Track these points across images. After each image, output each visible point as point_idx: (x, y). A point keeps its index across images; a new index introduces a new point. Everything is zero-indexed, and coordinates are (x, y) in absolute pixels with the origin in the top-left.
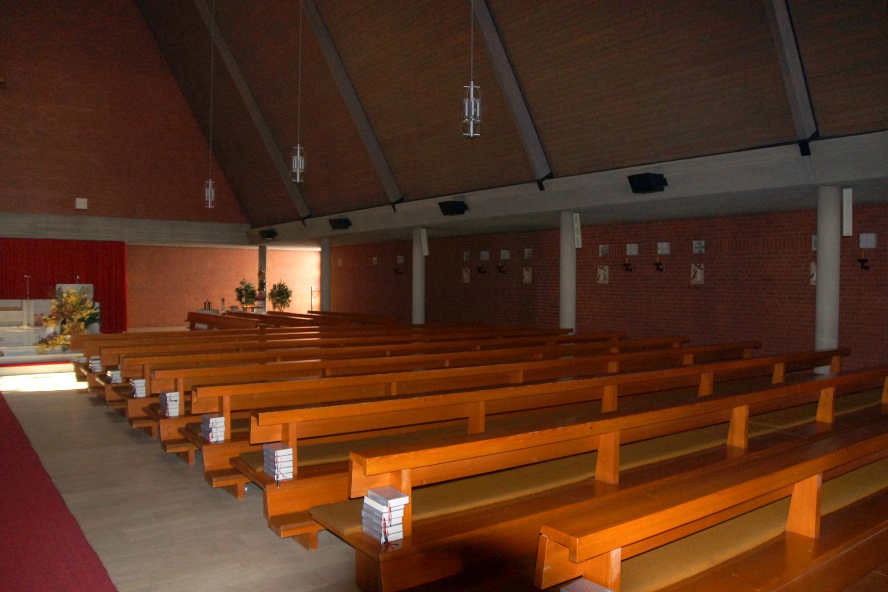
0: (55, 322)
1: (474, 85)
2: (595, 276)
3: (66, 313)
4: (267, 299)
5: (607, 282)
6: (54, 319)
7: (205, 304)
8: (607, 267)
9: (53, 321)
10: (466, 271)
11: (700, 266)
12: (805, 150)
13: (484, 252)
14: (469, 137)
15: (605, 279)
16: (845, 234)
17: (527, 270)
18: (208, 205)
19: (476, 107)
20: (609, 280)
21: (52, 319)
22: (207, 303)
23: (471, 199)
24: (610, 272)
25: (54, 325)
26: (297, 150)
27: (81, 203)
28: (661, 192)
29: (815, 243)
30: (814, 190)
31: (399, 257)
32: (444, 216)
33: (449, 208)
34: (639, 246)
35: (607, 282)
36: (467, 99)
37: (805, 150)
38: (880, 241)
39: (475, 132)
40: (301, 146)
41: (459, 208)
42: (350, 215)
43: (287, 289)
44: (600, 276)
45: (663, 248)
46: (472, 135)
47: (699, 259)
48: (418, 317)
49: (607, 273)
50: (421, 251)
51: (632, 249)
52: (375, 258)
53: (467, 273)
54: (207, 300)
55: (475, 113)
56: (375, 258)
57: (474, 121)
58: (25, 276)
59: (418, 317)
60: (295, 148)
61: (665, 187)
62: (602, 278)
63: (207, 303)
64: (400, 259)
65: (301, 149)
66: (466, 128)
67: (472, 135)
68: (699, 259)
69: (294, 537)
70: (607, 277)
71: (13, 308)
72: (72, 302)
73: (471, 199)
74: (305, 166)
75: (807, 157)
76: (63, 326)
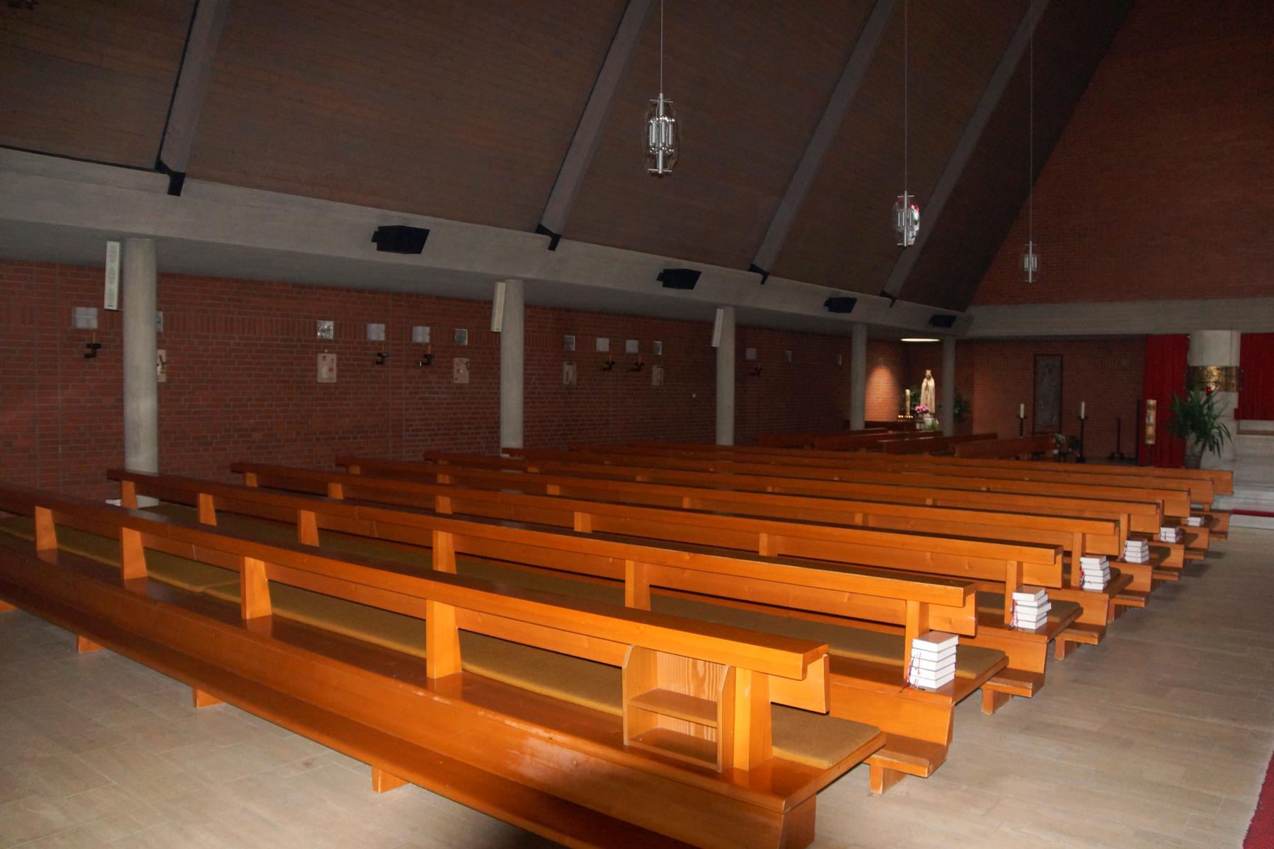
2: (313, 368)
4: (909, 397)
11: (1207, 414)
12: (175, 188)
14: (656, 174)
28: (416, 255)
29: (159, 322)
32: (694, 290)
33: (673, 278)
34: (595, 348)
39: (665, 166)
41: (685, 279)
42: (824, 313)
46: (660, 172)
48: (725, 435)
51: (377, 332)
57: (664, 152)
59: (725, 435)
60: (1026, 245)
61: (375, 245)
64: (751, 354)
67: (660, 172)
69: (1068, 627)
71: (758, 516)
75: (174, 197)
76: (632, 595)
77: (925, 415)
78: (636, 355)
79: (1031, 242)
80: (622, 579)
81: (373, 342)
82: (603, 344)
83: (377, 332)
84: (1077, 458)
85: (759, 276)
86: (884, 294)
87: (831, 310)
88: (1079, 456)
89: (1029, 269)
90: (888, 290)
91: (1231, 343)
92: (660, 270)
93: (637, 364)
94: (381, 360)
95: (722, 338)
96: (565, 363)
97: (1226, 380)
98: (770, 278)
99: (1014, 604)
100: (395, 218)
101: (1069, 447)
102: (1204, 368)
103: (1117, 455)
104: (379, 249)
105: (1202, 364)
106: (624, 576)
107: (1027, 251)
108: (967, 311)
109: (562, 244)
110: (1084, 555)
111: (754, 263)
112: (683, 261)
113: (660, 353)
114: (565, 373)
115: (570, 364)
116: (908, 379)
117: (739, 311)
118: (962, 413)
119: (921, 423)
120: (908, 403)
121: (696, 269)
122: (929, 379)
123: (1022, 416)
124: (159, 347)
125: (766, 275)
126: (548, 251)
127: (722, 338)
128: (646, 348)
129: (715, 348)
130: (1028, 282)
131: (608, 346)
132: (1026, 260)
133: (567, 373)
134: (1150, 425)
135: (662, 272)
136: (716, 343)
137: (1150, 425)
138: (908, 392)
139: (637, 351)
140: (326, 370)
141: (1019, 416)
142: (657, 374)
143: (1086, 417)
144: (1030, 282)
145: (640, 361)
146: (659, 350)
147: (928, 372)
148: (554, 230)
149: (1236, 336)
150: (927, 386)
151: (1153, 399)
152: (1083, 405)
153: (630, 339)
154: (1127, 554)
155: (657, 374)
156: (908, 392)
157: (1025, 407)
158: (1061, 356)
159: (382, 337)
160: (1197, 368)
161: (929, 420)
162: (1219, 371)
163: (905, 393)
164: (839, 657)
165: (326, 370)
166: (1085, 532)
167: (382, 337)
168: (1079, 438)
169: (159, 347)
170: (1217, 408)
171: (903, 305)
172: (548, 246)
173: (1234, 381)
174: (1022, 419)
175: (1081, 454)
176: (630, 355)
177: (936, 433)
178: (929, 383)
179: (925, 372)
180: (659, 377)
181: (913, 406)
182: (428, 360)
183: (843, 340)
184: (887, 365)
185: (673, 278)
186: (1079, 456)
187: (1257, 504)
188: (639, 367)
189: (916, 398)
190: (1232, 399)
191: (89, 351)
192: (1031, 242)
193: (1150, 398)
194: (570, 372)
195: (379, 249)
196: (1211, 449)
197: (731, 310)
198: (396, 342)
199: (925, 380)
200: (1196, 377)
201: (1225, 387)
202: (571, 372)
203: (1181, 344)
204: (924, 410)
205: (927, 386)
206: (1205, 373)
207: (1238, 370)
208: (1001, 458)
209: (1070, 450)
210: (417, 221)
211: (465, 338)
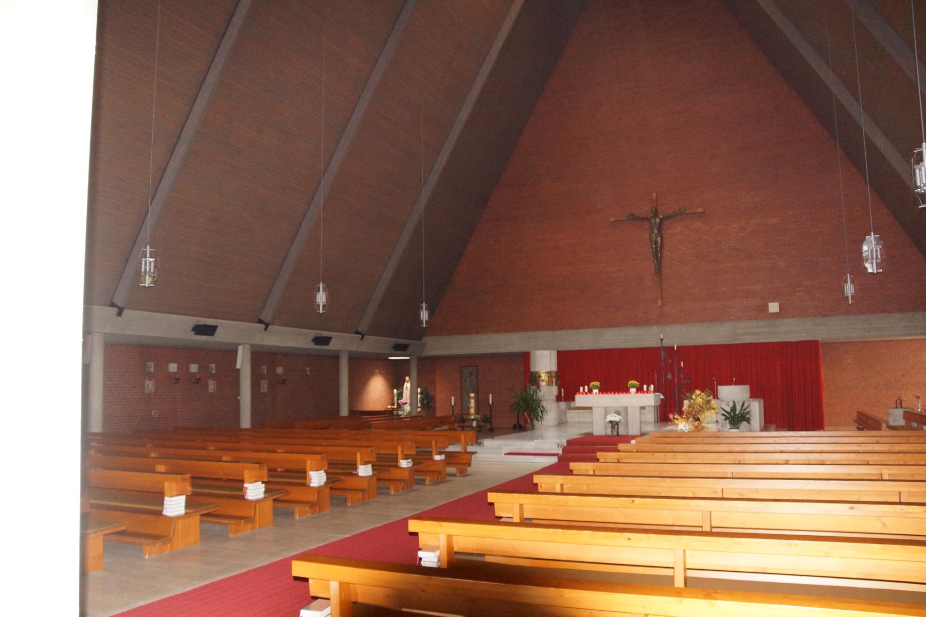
0: (685, 421)
1: (150, 248)
3: (694, 413)
6: (684, 418)
7: (896, 402)
9: (683, 420)
12: (119, 314)
18: (423, 324)
21: (682, 418)
22: (899, 401)
25: (684, 423)
26: (422, 306)
27: (774, 307)
33: (200, 330)
37: (119, 314)
38: (188, 368)
40: (425, 304)
41: (210, 330)
42: (313, 346)
43: (641, 393)
45: (194, 368)
48: (246, 422)
52: (264, 367)
54: (899, 397)
56: (264, 367)
58: (714, 379)
59: (246, 422)
62: (265, 386)
63: (899, 401)
65: (425, 306)
72: (699, 402)
74: (327, 300)
77: (405, 405)
78: (196, 373)
80: (709, 512)
82: (173, 367)
84: (489, 428)
85: (263, 326)
86: (357, 333)
88: (490, 427)
89: (423, 319)
90: (359, 330)
91: (550, 357)
92: (192, 325)
93: (283, 380)
95: (243, 362)
96: (146, 379)
97: (549, 379)
98: (270, 327)
99: (247, 488)
101: (482, 423)
102: (536, 372)
103: (517, 426)
105: (537, 370)
107: (846, 282)
108: (422, 340)
109: (126, 312)
110: (312, 470)
111: (260, 318)
112: (207, 319)
113: (214, 372)
114: (146, 385)
115: (150, 380)
116: (396, 383)
117: (252, 346)
118: (428, 402)
119: (402, 410)
120: (396, 398)
121: (214, 324)
122: (408, 382)
123: (453, 404)
125: (267, 325)
126: (116, 317)
127: (243, 362)
128: (204, 368)
129: (238, 370)
130: (423, 327)
131: (176, 369)
132: (853, 291)
133: (148, 385)
134: (472, 408)
135: (194, 326)
136: (238, 366)
137: (472, 408)
138: (395, 391)
139: (196, 371)
141: (451, 404)
142: (212, 386)
143: (455, 404)
144: (850, 303)
145: (285, 379)
146: (213, 369)
147: (407, 378)
148: (120, 305)
149: (554, 354)
150: (407, 387)
151: (473, 393)
152: (491, 395)
153: (192, 363)
154: (359, 472)
155: (212, 386)
156: (395, 391)
157: (455, 398)
158: (477, 367)
160: (532, 373)
161: (407, 408)
162: (544, 374)
163: (393, 391)
168: (489, 416)
170: (540, 394)
171: (370, 339)
172: (116, 314)
173: (554, 380)
174: (453, 406)
175: (491, 425)
176: (192, 373)
177: (411, 417)
178: (407, 385)
179: (405, 378)
180: (213, 387)
181: (398, 400)
182: (198, 381)
183: (335, 358)
184: (380, 374)
185: (200, 330)
186: (490, 427)
187: (520, 449)
188: (197, 380)
189: (400, 395)
190: (554, 390)
193: (471, 393)
194: (150, 385)
196: (537, 420)
197: (248, 347)
198: (902, 358)
199: (406, 383)
200: (534, 379)
201: (550, 383)
202: (150, 385)
203: (525, 358)
204: (404, 402)
205: (407, 387)
206: (537, 376)
207: (556, 373)
208: (419, 430)
209: (484, 424)
211: (152, 367)
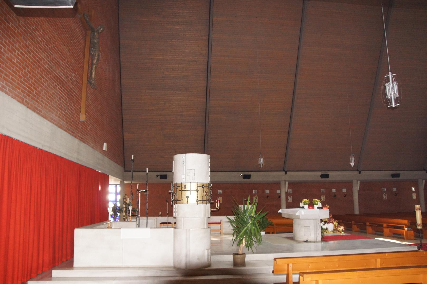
2: (382, 197)
5: (324, 201)
8: (324, 196)
10: (385, 195)
13: (269, 191)
15: (324, 199)
16: (280, 190)
17: (290, 197)
19: (262, 160)
20: (325, 200)
23: (331, 173)
24: (325, 198)
30: (352, 180)
31: (221, 191)
35: (324, 201)
36: (260, 158)
41: (327, 176)
42: (391, 178)
44: (322, 199)
47: (220, 195)
49: (324, 198)
50: (356, 188)
53: (386, 196)
55: (262, 162)
66: (353, 156)
68: (220, 195)
70: (325, 199)
73: (331, 173)
75: (251, 177)
79: (261, 154)
81: (333, 193)
83: (334, 190)
87: (392, 177)
94: (335, 196)
100: (394, 172)
104: (321, 178)
106: (142, 228)
124: (280, 194)
140: (385, 197)
141: (168, 203)
159: (335, 192)
164: (202, 279)
165: (385, 197)
166: (317, 279)
167: (335, 192)
169: (280, 194)
185: (393, 176)
191: (345, 196)
192: (261, 154)
195: (321, 178)
210: (398, 172)
